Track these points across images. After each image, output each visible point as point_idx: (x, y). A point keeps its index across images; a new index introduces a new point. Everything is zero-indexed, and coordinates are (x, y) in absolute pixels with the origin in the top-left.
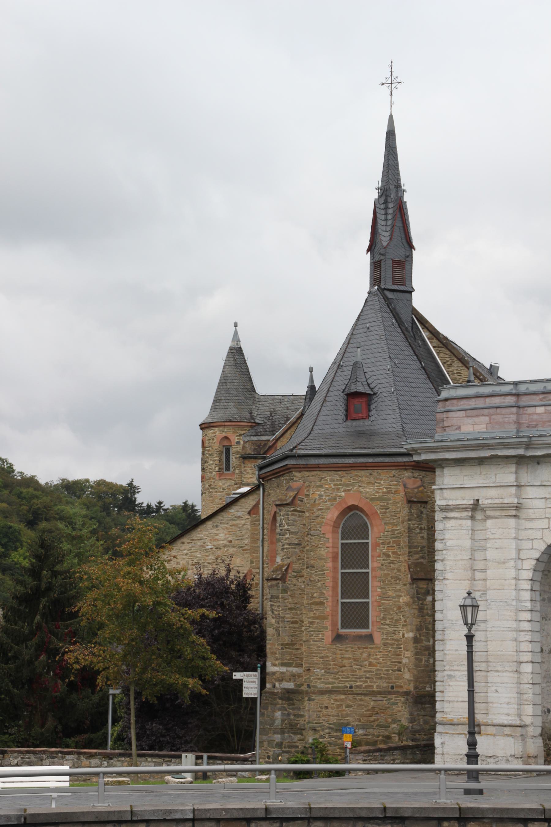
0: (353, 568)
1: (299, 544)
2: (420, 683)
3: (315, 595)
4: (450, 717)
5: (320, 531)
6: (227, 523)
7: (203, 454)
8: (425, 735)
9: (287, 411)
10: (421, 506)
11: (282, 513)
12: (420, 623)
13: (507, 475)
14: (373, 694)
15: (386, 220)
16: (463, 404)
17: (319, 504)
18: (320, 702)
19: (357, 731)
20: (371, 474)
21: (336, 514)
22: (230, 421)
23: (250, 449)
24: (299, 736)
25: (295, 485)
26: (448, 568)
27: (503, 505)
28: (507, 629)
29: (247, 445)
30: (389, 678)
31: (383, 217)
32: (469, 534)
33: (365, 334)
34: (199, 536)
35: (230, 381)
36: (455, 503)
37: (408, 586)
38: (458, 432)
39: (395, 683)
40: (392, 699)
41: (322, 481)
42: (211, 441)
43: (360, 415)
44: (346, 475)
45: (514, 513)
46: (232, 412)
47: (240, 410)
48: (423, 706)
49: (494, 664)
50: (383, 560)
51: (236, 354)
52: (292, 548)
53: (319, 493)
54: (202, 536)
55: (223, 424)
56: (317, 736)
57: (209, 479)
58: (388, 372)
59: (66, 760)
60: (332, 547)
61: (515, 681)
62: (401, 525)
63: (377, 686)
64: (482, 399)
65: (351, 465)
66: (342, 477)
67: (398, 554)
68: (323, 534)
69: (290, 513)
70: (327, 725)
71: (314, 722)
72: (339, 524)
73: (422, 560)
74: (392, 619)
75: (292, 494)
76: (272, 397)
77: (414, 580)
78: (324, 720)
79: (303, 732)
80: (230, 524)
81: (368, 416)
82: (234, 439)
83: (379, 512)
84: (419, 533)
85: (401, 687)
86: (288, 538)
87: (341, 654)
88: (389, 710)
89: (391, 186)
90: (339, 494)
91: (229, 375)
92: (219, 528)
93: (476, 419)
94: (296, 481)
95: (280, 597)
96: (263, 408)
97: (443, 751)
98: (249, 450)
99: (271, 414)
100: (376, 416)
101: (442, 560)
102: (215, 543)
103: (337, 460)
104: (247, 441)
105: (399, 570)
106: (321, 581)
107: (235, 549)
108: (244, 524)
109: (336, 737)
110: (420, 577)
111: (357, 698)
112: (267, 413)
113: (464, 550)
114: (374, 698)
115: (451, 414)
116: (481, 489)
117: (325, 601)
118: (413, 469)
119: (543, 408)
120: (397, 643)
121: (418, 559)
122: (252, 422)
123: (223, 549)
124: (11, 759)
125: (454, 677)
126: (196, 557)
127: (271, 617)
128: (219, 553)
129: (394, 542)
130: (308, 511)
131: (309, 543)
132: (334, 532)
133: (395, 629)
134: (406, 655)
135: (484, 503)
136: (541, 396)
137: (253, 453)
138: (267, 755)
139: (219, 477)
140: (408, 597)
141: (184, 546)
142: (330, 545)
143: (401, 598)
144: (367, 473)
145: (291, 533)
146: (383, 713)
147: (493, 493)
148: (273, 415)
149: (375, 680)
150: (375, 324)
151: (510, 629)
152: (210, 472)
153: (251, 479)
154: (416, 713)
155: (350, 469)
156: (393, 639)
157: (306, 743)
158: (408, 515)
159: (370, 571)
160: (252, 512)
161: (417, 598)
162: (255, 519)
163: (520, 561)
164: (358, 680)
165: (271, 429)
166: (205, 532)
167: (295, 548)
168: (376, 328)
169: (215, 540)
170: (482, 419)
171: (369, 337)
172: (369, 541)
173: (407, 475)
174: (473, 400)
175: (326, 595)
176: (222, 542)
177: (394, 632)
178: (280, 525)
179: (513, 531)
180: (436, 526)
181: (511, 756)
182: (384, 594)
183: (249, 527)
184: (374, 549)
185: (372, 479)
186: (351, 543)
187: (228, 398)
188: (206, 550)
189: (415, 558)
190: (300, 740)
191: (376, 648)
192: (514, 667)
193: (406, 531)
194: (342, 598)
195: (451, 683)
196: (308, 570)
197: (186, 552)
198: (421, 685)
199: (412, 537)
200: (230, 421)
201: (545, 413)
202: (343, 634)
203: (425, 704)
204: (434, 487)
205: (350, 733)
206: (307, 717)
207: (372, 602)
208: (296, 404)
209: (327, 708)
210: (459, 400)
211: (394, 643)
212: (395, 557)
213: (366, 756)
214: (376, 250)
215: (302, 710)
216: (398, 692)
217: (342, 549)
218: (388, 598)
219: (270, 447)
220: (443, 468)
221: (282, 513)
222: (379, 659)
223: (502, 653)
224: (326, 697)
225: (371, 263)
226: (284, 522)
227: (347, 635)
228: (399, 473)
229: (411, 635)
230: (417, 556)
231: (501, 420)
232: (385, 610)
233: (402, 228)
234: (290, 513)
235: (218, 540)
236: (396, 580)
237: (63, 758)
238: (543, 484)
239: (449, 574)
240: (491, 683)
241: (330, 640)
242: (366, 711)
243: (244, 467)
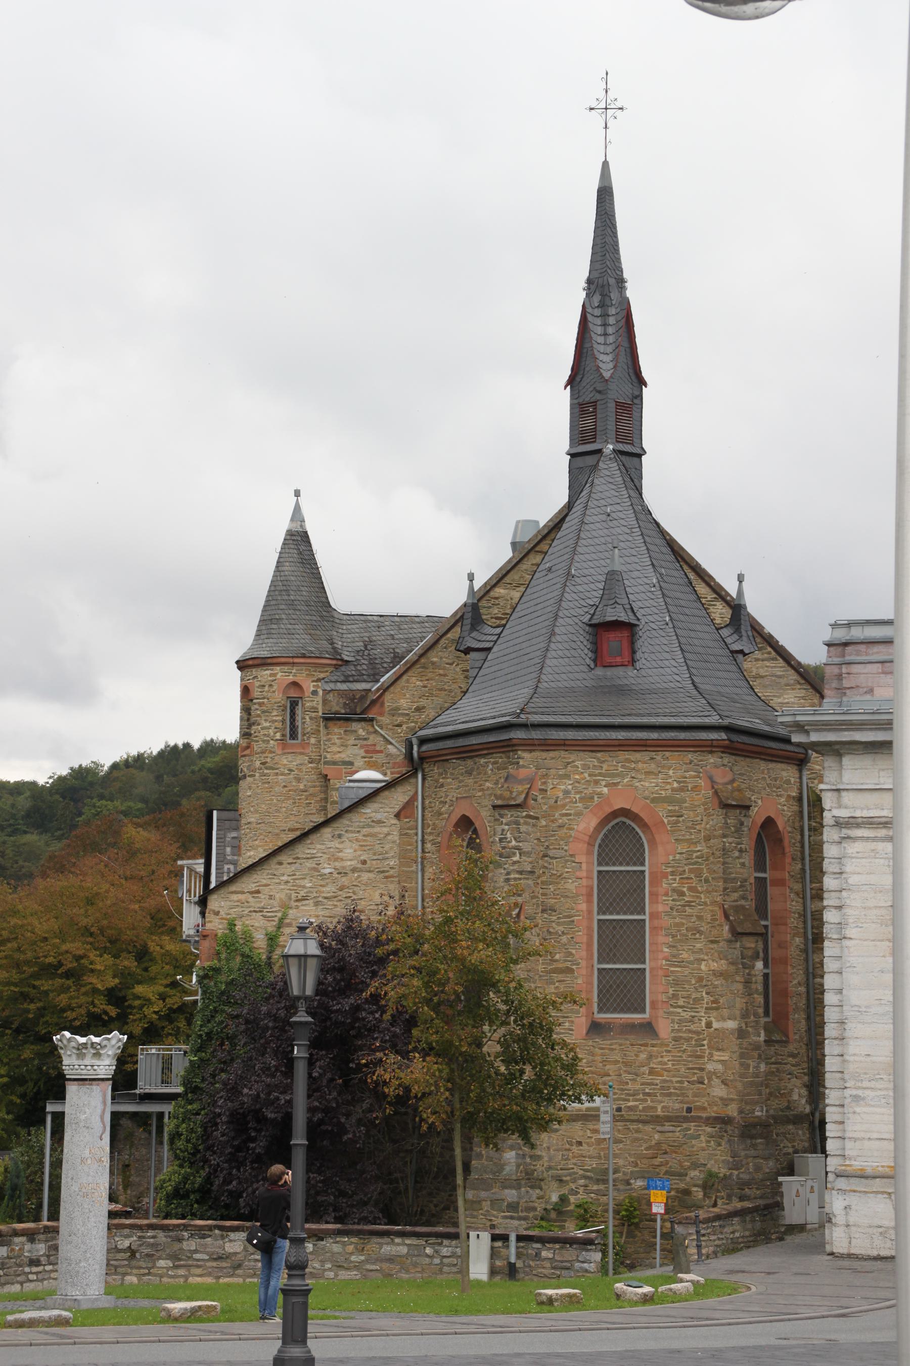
0: (618, 913)
1: (532, 872)
2: (746, 1103)
3: (557, 957)
4: (857, 1164)
5: (566, 851)
6: (359, 832)
8: (757, 1189)
9: (392, 641)
10: (740, 813)
11: (504, 821)
14: (657, 1120)
15: (605, 334)
16: (877, 653)
17: (564, 806)
18: (569, 1134)
19: (632, 1181)
20: (652, 759)
21: (594, 822)
22: (304, 656)
23: (337, 704)
24: (538, 1191)
25: (523, 773)
26: (851, 921)
29: (330, 697)
30: (683, 1095)
31: (599, 330)
32: (889, 866)
33: (604, 524)
34: (309, 851)
35: (295, 588)
36: (865, 813)
38: (868, 697)
39: (694, 1102)
40: (690, 1129)
41: (569, 768)
42: (266, 689)
43: (619, 659)
44: (610, 759)
46: (301, 640)
47: (315, 637)
48: (754, 1141)
50: (673, 900)
51: (298, 543)
52: (525, 878)
53: (563, 787)
54: (315, 851)
55: (291, 660)
56: (565, 1191)
57: (263, 752)
58: (653, 589)
59: (231, 1241)
60: (587, 878)
62: (704, 844)
63: (663, 1107)
65: (621, 742)
66: (604, 762)
67: (698, 892)
68: (571, 856)
69: (522, 821)
70: (581, 1172)
71: (559, 1167)
72: (595, 840)
73: (743, 902)
74: (688, 997)
76: (362, 618)
77: (737, 934)
78: (575, 1164)
79: (542, 1183)
80: (362, 833)
81: (633, 662)
82: (309, 686)
83: (666, 821)
84: (738, 858)
85: (704, 1109)
86: (518, 862)
87: (602, 1055)
88: (685, 1146)
89: (610, 279)
90: (599, 790)
91: (292, 578)
92: (344, 839)
94: (523, 766)
96: (349, 636)
97: (847, 1221)
98: (337, 706)
99: (366, 646)
101: (839, 908)
102: (337, 864)
103: (597, 734)
104: (330, 691)
106: (567, 934)
107: (371, 875)
108: (388, 834)
109: (597, 1192)
110: (748, 931)
111: (631, 1127)
112: (358, 644)
113: (881, 892)
114: (658, 1128)
115: (855, 669)
117: (574, 967)
118: (723, 752)
120: (696, 1037)
121: (737, 901)
122: (338, 659)
123: (350, 874)
124: (117, 1239)
125: (864, 1099)
126: (304, 887)
128: (345, 881)
129: (691, 871)
130: (544, 817)
131: (546, 871)
132: (589, 853)
133: (693, 1014)
134: (716, 1058)
137: (343, 711)
138: (488, 1224)
139: (283, 749)
141: (281, 869)
142: (584, 874)
143: (704, 963)
144: (646, 756)
146: (676, 1152)
148: (369, 647)
149: (659, 1098)
150: (619, 508)
152: (264, 741)
153: (339, 755)
154: (743, 1153)
156: (690, 1031)
157: (547, 1202)
160: (402, 813)
161: (743, 964)
162: (408, 825)
164: (631, 1098)
165: (371, 672)
166: (318, 846)
167: (527, 879)
168: (621, 515)
169: (336, 859)
171: (611, 530)
172: (646, 868)
173: (712, 761)
175: (577, 957)
176: (349, 863)
177: (692, 1020)
178: (501, 840)
180: (825, 851)
182: (674, 956)
183: (396, 838)
184: (655, 882)
185: (653, 766)
186: (614, 872)
187: (294, 617)
188: (321, 875)
189: (733, 899)
190: (538, 1198)
191: (662, 1045)
193: (718, 853)
194: (599, 962)
195: (858, 1110)
197: (285, 878)
198: (748, 1108)
199: (727, 863)
200: (304, 656)
202: (603, 1021)
203: (756, 1139)
204: (822, 786)
205: (663, 1189)
206: (546, 1159)
207: (652, 970)
208: (405, 631)
209: (580, 1143)
210: (870, 645)
211: (692, 1038)
212: (693, 896)
214: (583, 384)
215: (539, 1147)
216: (700, 1117)
217: (599, 881)
218: (681, 963)
219: (373, 702)
221: (504, 821)
222: (666, 1064)
224: (578, 1125)
225: (572, 405)
227: (610, 1023)
228: (700, 758)
229: (731, 1025)
230: (735, 895)
232: (677, 983)
233: (628, 350)
235: (342, 860)
236: (695, 934)
237: (223, 1237)
239: (854, 931)
241: (585, 1032)
242: (646, 1149)
243: (328, 734)
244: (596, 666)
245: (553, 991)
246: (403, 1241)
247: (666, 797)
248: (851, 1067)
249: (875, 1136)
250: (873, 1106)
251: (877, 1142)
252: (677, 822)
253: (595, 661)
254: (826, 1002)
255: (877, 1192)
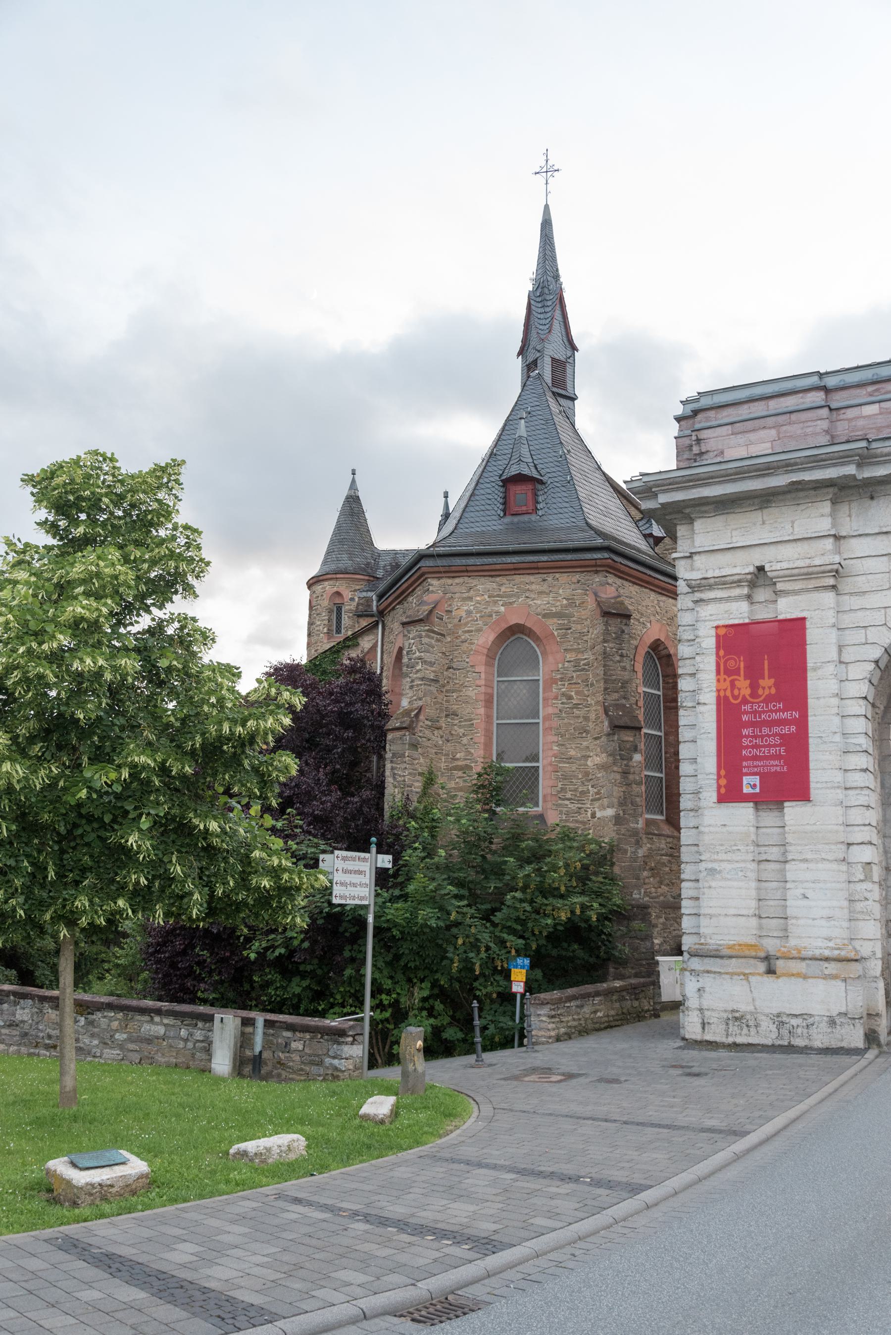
1: (436, 681)
3: (458, 756)
7: (310, 615)
10: (621, 622)
12: (624, 795)
13: (816, 518)
17: (466, 624)
20: (544, 580)
21: (492, 637)
25: (430, 598)
27: (810, 570)
28: (824, 785)
37: (604, 739)
43: (524, 508)
45: (831, 581)
49: (799, 848)
50: (562, 703)
53: (466, 608)
61: (844, 877)
64: (763, 403)
68: (472, 666)
69: (424, 634)
72: (496, 654)
74: (576, 790)
75: (427, 608)
82: (347, 594)
83: (556, 633)
84: (619, 662)
93: (752, 436)
94: (433, 592)
95: (407, 754)
100: (546, 509)
101: (693, 675)
105: (586, 719)
116: (766, 547)
118: (607, 571)
119: (877, 406)
125: (720, 872)
127: (391, 785)
132: (489, 664)
133: (580, 806)
135: (773, 568)
136: (870, 389)
140: (604, 755)
142: (482, 682)
143: (590, 759)
145: (425, 662)
147: (788, 551)
151: (829, 785)
155: (513, 572)
156: (577, 821)
158: (604, 634)
159: (540, 721)
161: (620, 755)
163: (843, 666)
170: (762, 433)
173: (597, 580)
174: (746, 406)
175: (475, 755)
177: (579, 811)
178: (408, 653)
179: (831, 613)
181: (840, 1014)
185: (545, 587)
192: (840, 851)
193: (600, 658)
195: (713, 884)
196: (449, 720)
201: (881, 414)
204: (674, 555)
207: (544, 767)
210: (718, 410)
213: (554, 1009)
220: (691, 521)
223: (815, 828)
226: (414, 648)
229: (610, 812)
230: (615, 696)
231: (799, 432)
232: (565, 777)
234: (424, 634)
237: (16, 1004)
238: (885, 530)
240: (793, 881)
244: (505, 514)
245: (453, 786)
246: (161, 1020)
247: (556, 613)
248: (707, 839)
249: (732, 911)
250: (729, 880)
251: (734, 919)
252: (566, 634)
253: (504, 511)
254: (681, 773)
255: (732, 974)
